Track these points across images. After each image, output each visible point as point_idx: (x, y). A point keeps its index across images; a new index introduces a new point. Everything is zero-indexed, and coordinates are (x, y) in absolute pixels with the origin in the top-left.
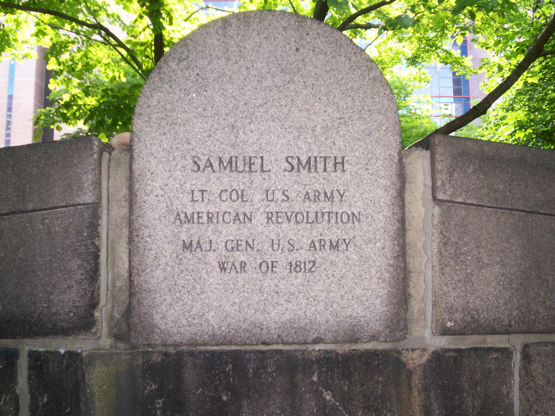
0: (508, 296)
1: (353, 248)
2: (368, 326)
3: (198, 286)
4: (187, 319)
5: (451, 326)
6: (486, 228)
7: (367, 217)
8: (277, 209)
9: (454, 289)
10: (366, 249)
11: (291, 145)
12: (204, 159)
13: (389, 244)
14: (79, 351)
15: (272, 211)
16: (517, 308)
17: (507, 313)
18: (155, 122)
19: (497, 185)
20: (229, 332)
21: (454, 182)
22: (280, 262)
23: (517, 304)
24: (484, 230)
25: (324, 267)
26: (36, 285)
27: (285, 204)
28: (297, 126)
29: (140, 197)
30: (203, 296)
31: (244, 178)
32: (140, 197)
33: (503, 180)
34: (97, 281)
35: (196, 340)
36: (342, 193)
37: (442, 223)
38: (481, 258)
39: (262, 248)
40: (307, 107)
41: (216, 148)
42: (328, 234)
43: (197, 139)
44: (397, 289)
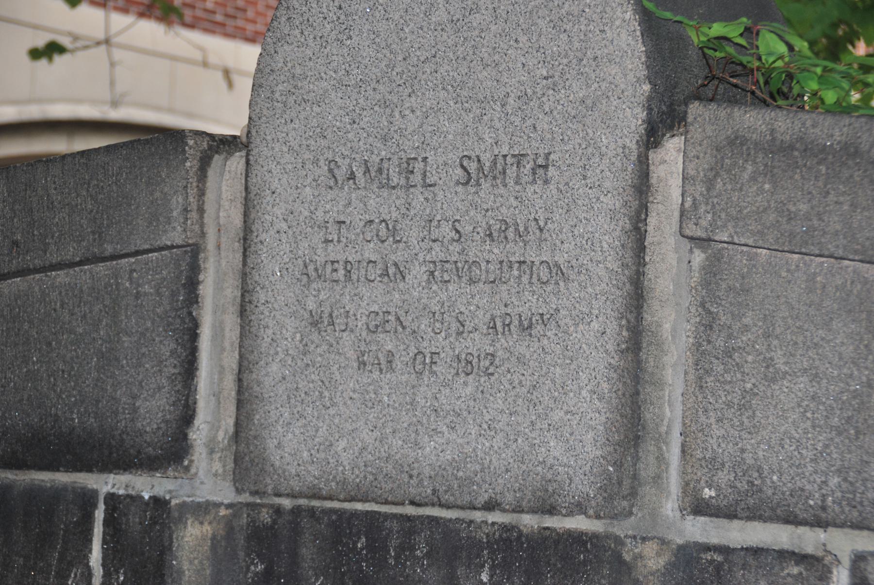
0: (821, 444)
1: (554, 331)
2: (570, 484)
3: (326, 394)
4: (309, 451)
5: (711, 497)
6: (786, 297)
7: (579, 273)
8: (442, 256)
9: (719, 420)
10: (574, 335)
11: (468, 135)
12: (344, 164)
13: (612, 327)
14: (167, 498)
15: (435, 259)
16: (839, 471)
17: (818, 480)
18: (280, 99)
19: (795, 204)
20: (365, 477)
21: (715, 200)
22: (442, 355)
23: (839, 463)
24: (783, 300)
25: (507, 365)
26: (119, 383)
27: (456, 248)
28: (481, 97)
29: (255, 234)
30: (332, 411)
31: (398, 198)
32: (255, 234)
33: (810, 193)
34: (193, 379)
35: (320, 489)
36: (542, 224)
37: (706, 284)
38: (772, 359)
39: (418, 328)
40: (496, 57)
41: (361, 143)
42: (516, 303)
43: (335, 129)
44: (622, 416)
